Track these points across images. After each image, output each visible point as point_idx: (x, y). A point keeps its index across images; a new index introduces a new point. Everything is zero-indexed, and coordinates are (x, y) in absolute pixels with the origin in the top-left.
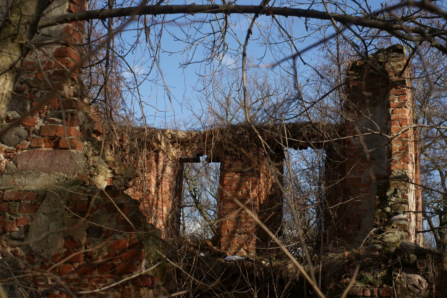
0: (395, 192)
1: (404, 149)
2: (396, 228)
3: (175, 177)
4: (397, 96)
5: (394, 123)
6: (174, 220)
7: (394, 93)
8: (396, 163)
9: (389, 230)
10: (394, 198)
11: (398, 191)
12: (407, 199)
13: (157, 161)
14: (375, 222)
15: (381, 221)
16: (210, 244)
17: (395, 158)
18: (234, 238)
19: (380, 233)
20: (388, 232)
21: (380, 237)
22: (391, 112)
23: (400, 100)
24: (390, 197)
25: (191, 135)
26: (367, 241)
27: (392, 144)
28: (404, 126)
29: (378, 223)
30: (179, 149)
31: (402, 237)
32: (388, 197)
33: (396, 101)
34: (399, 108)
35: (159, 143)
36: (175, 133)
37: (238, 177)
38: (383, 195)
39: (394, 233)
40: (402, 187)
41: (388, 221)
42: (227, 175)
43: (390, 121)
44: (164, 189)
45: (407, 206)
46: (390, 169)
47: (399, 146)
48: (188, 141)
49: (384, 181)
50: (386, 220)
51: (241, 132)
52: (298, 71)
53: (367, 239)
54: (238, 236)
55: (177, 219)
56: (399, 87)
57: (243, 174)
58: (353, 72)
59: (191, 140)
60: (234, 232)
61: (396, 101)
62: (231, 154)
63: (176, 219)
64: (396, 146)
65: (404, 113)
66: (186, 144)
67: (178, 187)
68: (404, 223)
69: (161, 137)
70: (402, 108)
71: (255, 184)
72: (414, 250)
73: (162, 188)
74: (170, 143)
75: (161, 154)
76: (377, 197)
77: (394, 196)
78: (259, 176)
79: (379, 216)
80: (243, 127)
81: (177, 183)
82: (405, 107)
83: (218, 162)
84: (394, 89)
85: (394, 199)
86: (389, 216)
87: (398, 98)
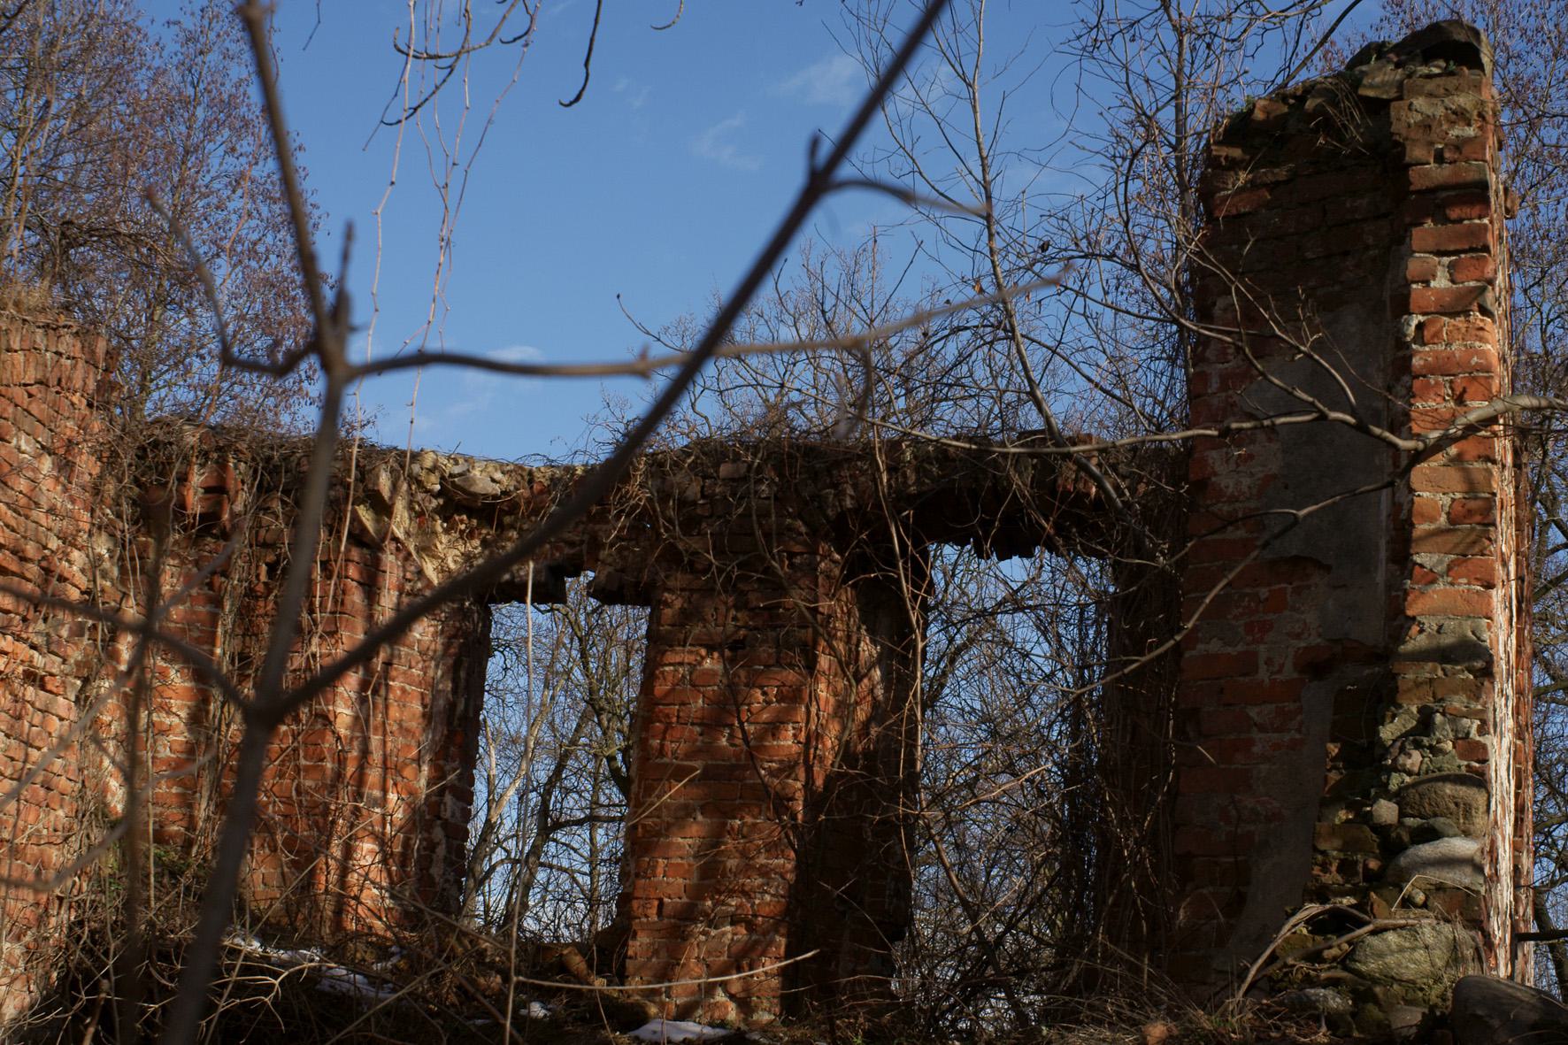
0: (1426, 723)
1: (1470, 513)
2: (1425, 905)
3: (450, 661)
4: (1446, 260)
5: (1428, 387)
6: (433, 851)
7: (1431, 244)
8: (1433, 581)
9: (1391, 916)
10: (1416, 756)
11: (1438, 718)
12: (1484, 761)
13: (371, 587)
14: (1316, 871)
15: (1346, 868)
16: (578, 962)
17: (1425, 558)
18: (685, 939)
19: (1341, 931)
20: (1381, 922)
21: (1337, 946)
22: (1411, 330)
23: (1458, 277)
24: (1395, 751)
25: (531, 481)
26: (1270, 970)
27: (1411, 491)
28: (1476, 404)
29: (1332, 877)
30: (476, 542)
31: (1455, 958)
32: (1387, 750)
33: (1441, 282)
34: (1453, 314)
35: (383, 509)
36: (457, 470)
37: (719, 667)
38: (1364, 741)
39: (1413, 930)
40: (1457, 703)
41: (1382, 865)
42: (671, 657)
43: (1406, 378)
44: (394, 712)
45: (1481, 798)
46: (1403, 611)
47: (1446, 500)
48: (513, 507)
49: (1367, 672)
50: (1373, 864)
51: (743, 469)
52: (995, 194)
53: (1273, 958)
54: (704, 933)
55: (449, 848)
56: (1454, 213)
57: (735, 649)
58: (1237, 153)
59: (528, 503)
60: (688, 915)
61: (1441, 282)
62: (691, 563)
63: (441, 851)
64: (1434, 493)
65: (1480, 337)
66: (507, 519)
67: (461, 707)
68: (1467, 881)
69: (395, 488)
70: (1466, 313)
71: (792, 696)
72: (1534, 1026)
73: (387, 707)
74: (436, 511)
75: (390, 560)
76: (1334, 749)
77: (1418, 746)
78: (811, 665)
79: (1337, 843)
80: (755, 449)
81: (455, 691)
82: (1485, 311)
83: (643, 604)
84: (1429, 224)
85: (1415, 759)
86: (1391, 844)
87: (1451, 266)
